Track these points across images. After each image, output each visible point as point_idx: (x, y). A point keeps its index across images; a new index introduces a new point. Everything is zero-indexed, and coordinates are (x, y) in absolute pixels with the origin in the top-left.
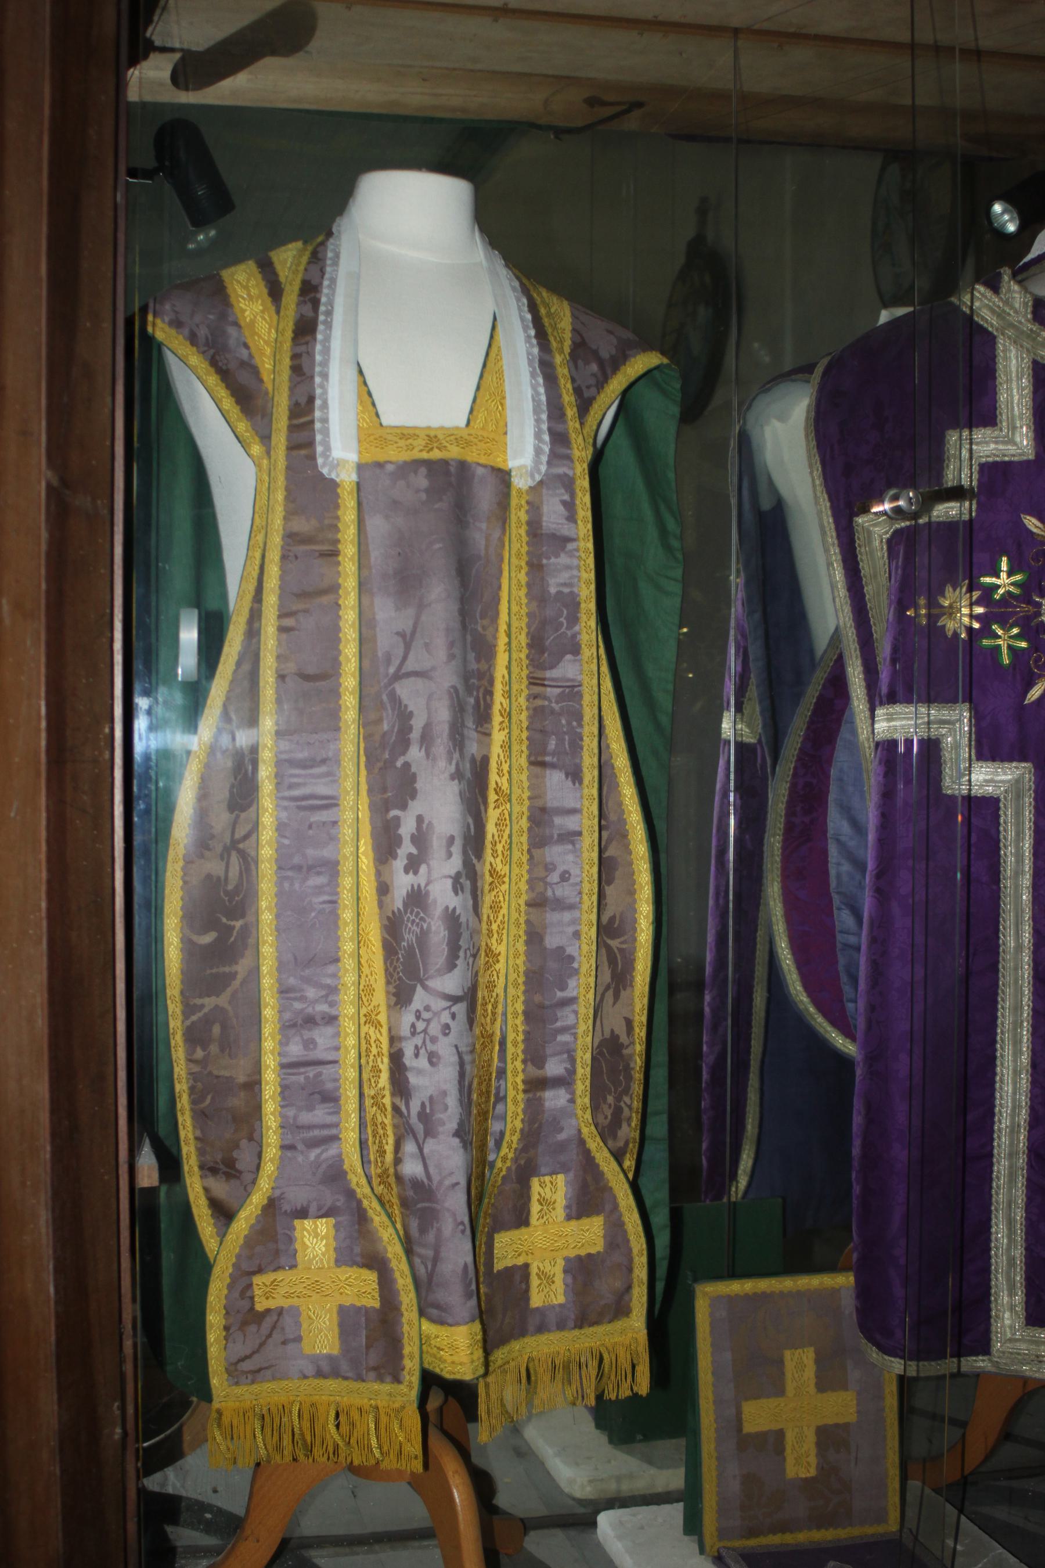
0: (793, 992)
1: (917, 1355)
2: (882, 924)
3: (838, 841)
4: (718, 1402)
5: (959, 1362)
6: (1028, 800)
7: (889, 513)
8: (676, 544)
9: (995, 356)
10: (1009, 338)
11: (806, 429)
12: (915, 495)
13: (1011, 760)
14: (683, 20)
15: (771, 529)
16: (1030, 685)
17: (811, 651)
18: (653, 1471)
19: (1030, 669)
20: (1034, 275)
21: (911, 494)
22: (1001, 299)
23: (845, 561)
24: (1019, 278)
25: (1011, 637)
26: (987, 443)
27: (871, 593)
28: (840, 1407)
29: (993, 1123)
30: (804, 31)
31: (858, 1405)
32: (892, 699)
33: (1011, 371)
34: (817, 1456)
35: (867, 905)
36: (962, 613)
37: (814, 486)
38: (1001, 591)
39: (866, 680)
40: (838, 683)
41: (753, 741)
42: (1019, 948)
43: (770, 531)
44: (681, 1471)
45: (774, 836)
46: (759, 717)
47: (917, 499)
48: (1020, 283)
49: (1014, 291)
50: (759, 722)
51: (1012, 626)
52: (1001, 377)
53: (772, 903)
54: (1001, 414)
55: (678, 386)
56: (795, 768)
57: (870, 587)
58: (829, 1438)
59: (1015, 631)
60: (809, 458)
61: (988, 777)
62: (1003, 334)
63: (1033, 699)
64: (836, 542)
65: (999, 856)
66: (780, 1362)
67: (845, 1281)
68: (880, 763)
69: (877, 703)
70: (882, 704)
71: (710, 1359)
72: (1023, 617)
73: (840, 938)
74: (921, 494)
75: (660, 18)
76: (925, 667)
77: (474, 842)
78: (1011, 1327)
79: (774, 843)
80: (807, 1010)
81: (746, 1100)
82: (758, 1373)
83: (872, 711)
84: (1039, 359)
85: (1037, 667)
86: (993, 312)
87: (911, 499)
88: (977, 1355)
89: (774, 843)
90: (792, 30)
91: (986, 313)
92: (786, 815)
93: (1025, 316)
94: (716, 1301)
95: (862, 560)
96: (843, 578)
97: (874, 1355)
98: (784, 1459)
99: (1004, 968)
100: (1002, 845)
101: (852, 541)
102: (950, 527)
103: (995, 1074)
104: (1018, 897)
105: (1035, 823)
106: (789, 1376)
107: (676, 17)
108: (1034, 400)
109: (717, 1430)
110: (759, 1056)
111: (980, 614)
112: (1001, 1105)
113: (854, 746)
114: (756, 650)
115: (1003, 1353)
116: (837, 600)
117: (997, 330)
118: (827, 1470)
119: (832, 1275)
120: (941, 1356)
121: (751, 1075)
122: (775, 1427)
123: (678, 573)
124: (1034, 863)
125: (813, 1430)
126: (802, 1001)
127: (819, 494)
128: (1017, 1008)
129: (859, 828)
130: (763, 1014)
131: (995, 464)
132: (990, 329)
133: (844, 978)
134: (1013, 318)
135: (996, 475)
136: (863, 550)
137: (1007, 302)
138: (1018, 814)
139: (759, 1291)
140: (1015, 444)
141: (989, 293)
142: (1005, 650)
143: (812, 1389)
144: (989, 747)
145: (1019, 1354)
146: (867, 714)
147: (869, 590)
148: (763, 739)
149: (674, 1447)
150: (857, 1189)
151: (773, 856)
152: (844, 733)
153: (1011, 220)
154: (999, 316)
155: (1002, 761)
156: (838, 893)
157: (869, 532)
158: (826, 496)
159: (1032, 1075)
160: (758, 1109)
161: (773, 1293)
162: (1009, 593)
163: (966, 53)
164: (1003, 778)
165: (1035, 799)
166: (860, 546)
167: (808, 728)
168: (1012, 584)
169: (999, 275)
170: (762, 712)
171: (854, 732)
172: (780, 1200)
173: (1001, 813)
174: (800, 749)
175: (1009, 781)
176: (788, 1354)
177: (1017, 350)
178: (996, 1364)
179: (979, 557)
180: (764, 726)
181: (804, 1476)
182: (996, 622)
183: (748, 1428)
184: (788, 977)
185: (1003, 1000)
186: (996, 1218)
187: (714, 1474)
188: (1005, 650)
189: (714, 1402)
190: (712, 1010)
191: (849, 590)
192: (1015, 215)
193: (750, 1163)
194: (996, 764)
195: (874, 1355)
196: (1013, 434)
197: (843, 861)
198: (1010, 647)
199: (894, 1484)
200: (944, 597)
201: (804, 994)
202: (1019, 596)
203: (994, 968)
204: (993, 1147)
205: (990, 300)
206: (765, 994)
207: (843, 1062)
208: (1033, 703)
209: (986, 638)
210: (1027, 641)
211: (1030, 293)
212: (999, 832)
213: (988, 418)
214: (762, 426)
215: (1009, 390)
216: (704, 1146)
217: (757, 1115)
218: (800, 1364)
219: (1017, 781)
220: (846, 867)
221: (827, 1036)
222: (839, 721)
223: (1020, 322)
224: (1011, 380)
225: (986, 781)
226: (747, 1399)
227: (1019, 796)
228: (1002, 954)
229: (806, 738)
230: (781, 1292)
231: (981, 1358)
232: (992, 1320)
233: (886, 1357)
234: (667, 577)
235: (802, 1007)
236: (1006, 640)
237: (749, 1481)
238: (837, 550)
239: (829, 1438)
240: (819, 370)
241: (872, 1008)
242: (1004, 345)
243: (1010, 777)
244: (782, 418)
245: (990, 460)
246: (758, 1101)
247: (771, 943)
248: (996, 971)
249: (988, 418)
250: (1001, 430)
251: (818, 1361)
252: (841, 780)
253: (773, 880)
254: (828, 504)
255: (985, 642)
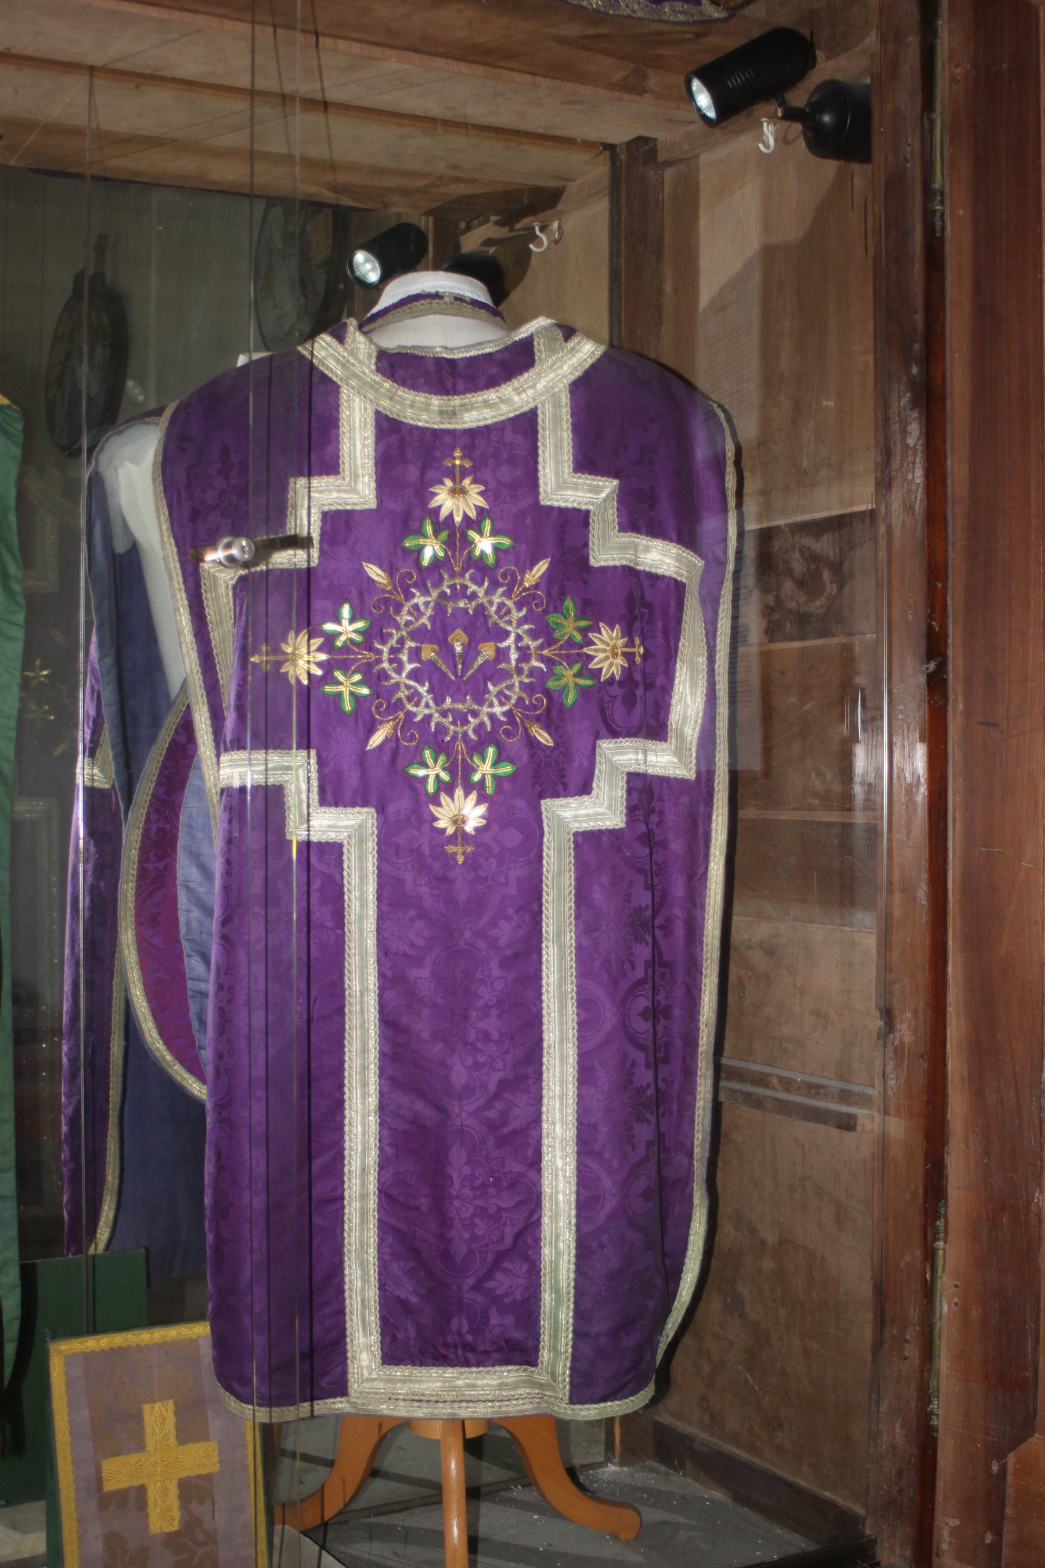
0: (149, 1040)
1: (269, 1401)
2: (227, 973)
3: (188, 889)
4: (77, 1463)
5: (312, 1406)
6: (372, 845)
7: (223, 561)
8: (17, 587)
9: (339, 406)
10: (353, 388)
11: (154, 472)
12: (248, 545)
13: (353, 804)
14: (36, 55)
15: (125, 572)
16: (371, 731)
17: (167, 695)
18: (17, 1536)
19: (372, 716)
20: (381, 327)
21: (244, 543)
22: (346, 350)
23: (191, 606)
24: (365, 329)
25: (353, 684)
26: (330, 491)
27: (217, 638)
28: (202, 1458)
29: (343, 1166)
30: (160, 73)
31: (220, 1454)
32: (239, 744)
33: (354, 421)
34: (180, 1509)
35: (215, 951)
36: (304, 659)
37: (161, 531)
38: (343, 638)
39: (212, 725)
40: (187, 727)
41: (107, 786)
42: (364, 991)
43: (124, 575)
44: (43, 1535)
45: (127, 882)
46: (113, 763)
47: (250, 548)
48: (365, 334)
49: (359, 342)
50: (112, 767)
51: (355, 672)
52: (344, 428)
53: (126, 951)
54: (344, 463)
55: (19, 427)
56: (148, 814)
57: (216, 633)
58: (192, 1490)
59: (357, 677)
60: (156, 502)
61: (331, 823)
62: (347, 384)
63: (374, 745)
64: (183, 587)
65: (343, 901)
66: (139, 1417)
67: (201, 1331)
68: (225, 810)
69: (222, 749)
70: (226, 750)
71: (66, 1419)
72: (366, 663)
73: (190, 984)
74: (255, 543)
75: (13, 51)
76: (269, 714)
77: (309, 791)
78: (369, 1367)
79: (128, 890)
80: (163, 1057)
81: (105, 1150)
82: (117, 1429)
83: (218, 756)
84: (381, 410)
85: (379, 713)
86: (337, 361)
87: (243, 547)
88: (335, 1396)
89: (128, 890)
90: (148, 71)
91: (331, 363)
92: (140, 862)
93: (369, 367)
94: (70, 1360)
95: (208, 606)
96: (189, 624)
97: (233, 1404)
98: (147, 1515)
99: (350, 1012)
100: (345, 889)
101: (198, 586)
102: (287, 574)
103: (344, 1117)
104: (362, 941)
105: (378, 868)
106: (148, 1430)
107: (29, 51)
108: (376, 451)
109: (76, 1490)
110: (118, 1106)
111: (323, 661)
112: (350, 1147)
113: (201, 792)
114: (108, 694)
115: (361, 1393)
116: (184, 646)
117: (341, 380)
118: (190, 1524)
119: (190, 1325)
120: (290, 1400)
121: (110, 1125)
122: (136, 1483)
123: (20, 618)
124: (378, 907)
125: (175, 1483)
126: (158, 1048)
127: (166, 539)
128: (364, 1050)
129: (206, 873)
130: (120, 1063)
131: (338, 513)
132: (335, 379)
133: (195, 1025)
134: (358, 369)
135: (339, 524)
136: (209, 596)
137: (351, 353)
138: (362, 858)
139: (115, 1346)
140: (357, 492)
141: (334, 343)
142: (346, 696)
143: (173, 1441)
144: (332, 793)
145: (376, 1393)
146: (215, 760)
147: (215, 636)
148: (116, 785)
149: (36, 1510)
150: (210, 1238)
151: (126, 903)
152: (192, 780)
153: (373, 270)
154: (343, 366)
155: (345, 806)
156: (188, 940)
157: (215, 578)
158: (173, 541)
159: (380, 1117)
160: (118, 1160)
161: (129, 1347)
162: (351, 640)
163: (310, 104)
164: (347, 823)
165: (378, 844)
166: (206, 592)
167: (161, 773)
168: (354, 631)
169: (345, 325)
170: (115, 758)
171: (202, 778)
172: (143, 1250)
173: (345, 857)
174: (153, 795)
175: (352, 826)
176: (146, 1408)
177: (361, 400)
178: (354, 1405)
179: (318, 604)
180: (117, 772)
181: (168, 1531)
182: (339, 669)
183: (109, 1486)
184: (144, 1025)
185: (350, 1043)
186: (350, 1259)
187: (75, 1536)
188: (346, 696)
189: (73, 1463)
190: (69, 1060)
191: (196, 635)
192: (377, 266)
193: (111, 1216)
194: (340, 809)
195: (233, 1404)
196: (356, 482)
197: (193, 908)
198: (352, 693)
199: (262, 1532)
200: (287, 643)
201: (161, 1042)
202: (361, 643)
203: (340, 1011)
204: (343, 1190)
205: (335, 350)
206: (123, 1043)
207: (200, 1106)
208: (374, 749)
209: (329, 684)
210: (370, 687)
211: (375, 344)
212: (342, 877)
213: (331, 467)
214: (116, 469)
215: (352, 439)
216: (65, 1198)
217: (117, 1165)
218: (159, 1418)
219: (360, 826)
220: (196, 914)
221: (185, 1084)
222: (189, 766)
223: (364, 373)
224: (354, 430)
225: (330, 827)
226: (106, 1457)
227: (361, 841)
228: (347, 997)
229: (159, 783)
230: (138, 1346)
231: (339, 1399)
232: (349, 1361)
233: (244, 1405)
234: (8, 621)
235: (158, 1055)
236: (349, 687)
237: (113, 1541)
238: (184, 595)
239: (192, 1490)
240: (168, 414)
241: (219, 1056)
242: (348, 396)
243: (353, 822)
244: (136, 461)
245: (333, 508)
246: (118, 1150)
247: (127, 990)
248: (343, 1014)
249: (331, 467)
250: (344, 478)
251: (177, 1414)
252: (190, 826)
253: (126, 928)
254: (175, 549)
255: (329, 689)
